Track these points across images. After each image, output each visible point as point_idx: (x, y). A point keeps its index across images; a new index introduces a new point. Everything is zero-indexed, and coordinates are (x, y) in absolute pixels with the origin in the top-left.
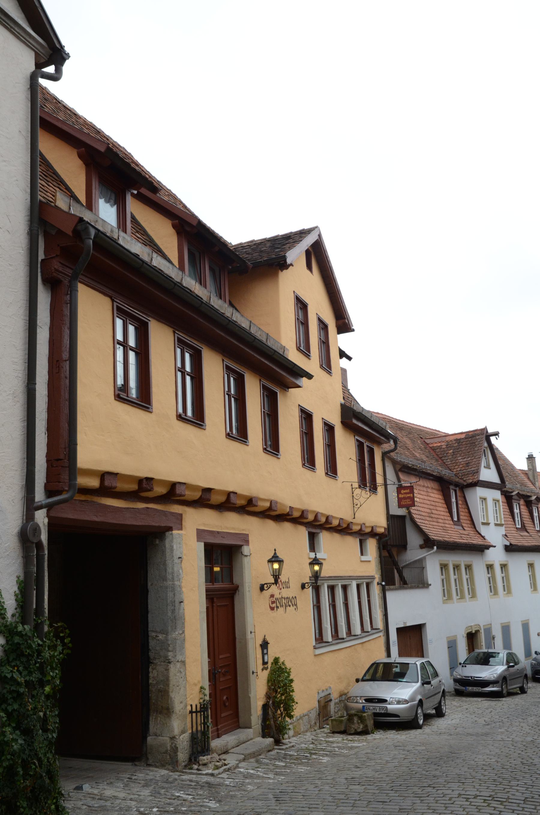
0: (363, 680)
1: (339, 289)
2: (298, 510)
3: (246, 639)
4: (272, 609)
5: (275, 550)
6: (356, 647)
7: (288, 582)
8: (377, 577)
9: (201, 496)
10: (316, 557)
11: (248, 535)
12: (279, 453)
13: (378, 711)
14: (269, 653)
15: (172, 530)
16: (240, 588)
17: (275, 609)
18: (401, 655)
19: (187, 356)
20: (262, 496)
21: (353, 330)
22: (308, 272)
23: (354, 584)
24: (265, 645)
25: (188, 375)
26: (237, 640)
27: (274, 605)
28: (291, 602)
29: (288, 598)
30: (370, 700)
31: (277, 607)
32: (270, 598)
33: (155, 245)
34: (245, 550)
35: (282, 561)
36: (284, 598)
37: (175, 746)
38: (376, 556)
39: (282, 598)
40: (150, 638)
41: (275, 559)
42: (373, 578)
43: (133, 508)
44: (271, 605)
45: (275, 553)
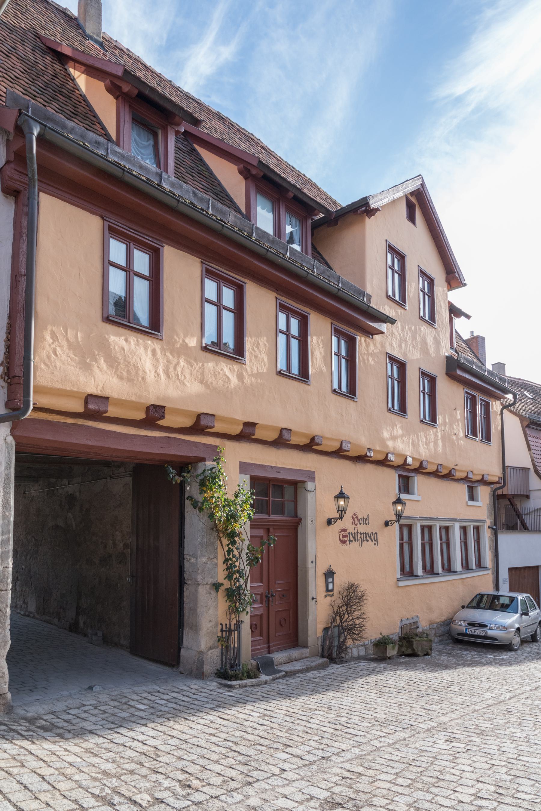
0: (468, 607)
1: (448, 242)
2: (446, 468)
3: (306, 567)
4: (343, 542)
5: (342, 487)
6: (475, 578)
7: (368, 519)
8: (489, 522)
9: (242, 430)
10: (399, 497)
11: (315, 472)
12: (355, 396)
13: (479, 634)
14: (335, 582)
15: (205, 461)
16: (303, 521)
17: (348, 542)
18: (511, 590)
19: (395, 368)
20: (328, 435)
21: (465, 285)
22: (410, 224)
23: (457, 526)
24: (329, 574)
25: (343, 358)
26: (299, 568)
27: (346, 539)
28: (372, 537)
29: (366, 533)
30: (472, 624)
31: (350, 541)
32: (341, 532)
33: (227, 196)
34: (310, 486)
35: (348, 497)
36: (361, 533)
37: (202, 659)
38: (488, 502)
39: (357, 533)
40: (185, 561)
41: (341, 495)
42: (484, 521)
43: (146, 436)
44: (342, 539)
45: (342, 490)
